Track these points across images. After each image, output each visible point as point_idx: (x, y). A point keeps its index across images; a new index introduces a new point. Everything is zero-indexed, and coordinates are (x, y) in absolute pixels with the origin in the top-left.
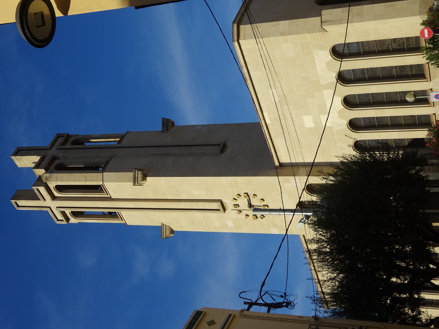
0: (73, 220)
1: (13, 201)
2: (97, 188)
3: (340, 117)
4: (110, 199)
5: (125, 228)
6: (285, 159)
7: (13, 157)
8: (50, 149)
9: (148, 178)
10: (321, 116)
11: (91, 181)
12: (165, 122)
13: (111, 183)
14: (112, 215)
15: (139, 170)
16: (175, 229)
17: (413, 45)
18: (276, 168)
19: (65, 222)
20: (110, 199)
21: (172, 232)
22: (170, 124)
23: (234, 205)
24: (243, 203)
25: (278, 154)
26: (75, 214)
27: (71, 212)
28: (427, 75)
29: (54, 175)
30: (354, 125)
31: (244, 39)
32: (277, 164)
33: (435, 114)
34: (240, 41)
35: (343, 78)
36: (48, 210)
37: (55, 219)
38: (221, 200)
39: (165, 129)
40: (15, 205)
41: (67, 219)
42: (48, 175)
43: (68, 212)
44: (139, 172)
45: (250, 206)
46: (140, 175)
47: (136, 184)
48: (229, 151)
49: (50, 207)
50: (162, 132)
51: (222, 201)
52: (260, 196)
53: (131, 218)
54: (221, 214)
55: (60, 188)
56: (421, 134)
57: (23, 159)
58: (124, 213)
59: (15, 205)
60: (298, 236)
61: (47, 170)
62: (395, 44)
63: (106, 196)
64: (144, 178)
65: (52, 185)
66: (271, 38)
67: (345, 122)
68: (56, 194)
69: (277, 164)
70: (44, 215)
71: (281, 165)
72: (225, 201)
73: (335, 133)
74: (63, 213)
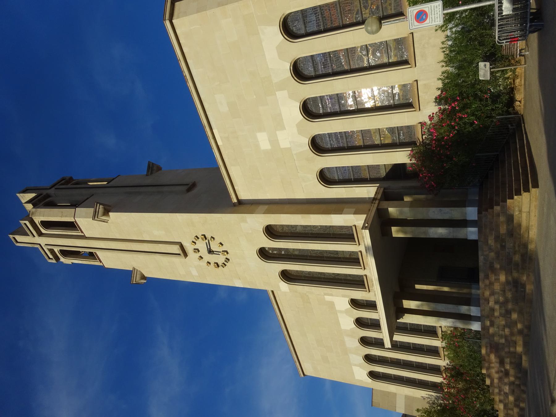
0: (62, 259)
1: (11, 236)
2: (72, 226)
3: (295, 132)
4: (84, 237)
5: (102, 268)
6: (244, 195)
7: (18, 195)
8: (50, 188)
9: (111, 214)
10: (277, 132)
11: (66, 216)
12: (151, 166)
13: (81, 219)
14: (92, 256)
15: (100, 204)
16: (146, 275)
17: (391, 9)
18: (234, 205)
19: (54, 261)
20: (84, 237)
21: (143, 277)
22: (155, 168)
23: (195, 249)
24: (201, 245)
25: (236, 188)
26: (65, 253)
27: (60, 250)
28: (412, 61)
29: (39, 210)
30: (318, 146)
31: (178, 17)
32: (235, 200)
33: (417, 81)
34: (173, 21)
35: (300, 72)
36: (38, 246)
37: (46, 257)
38: (181, 243)
39: (150, 172)
40: (13, 240)
41: (57, 258)
42: (34, 210)
43: (56, 250)
44: (101, 206)
45: (210, 251)
46: (101, 209)
47: (96, 219)
48: (195, 191)
49: (40, 245)
50: (147, 175)
51: (181, 244)
52: (218, 240)
53: (110, 261)
54: (181, 259)
55: (47, 225)
56: (402, 157)
57: (24, 196)
58: (100, 254)
59: (13, 240)
60: (266, 291)
61: (35, 206)
62: (367, 11)
63: (81, 234)
64: (106, 212)
65: (37, 220)
66: (207, 11)
67: (305, 141)
68: (43, 231)
69: (235, 200)
70: (33, 253)
71: (240, 202)
72: (185, 244)
73: (295, 158)
74: (52, 251)
